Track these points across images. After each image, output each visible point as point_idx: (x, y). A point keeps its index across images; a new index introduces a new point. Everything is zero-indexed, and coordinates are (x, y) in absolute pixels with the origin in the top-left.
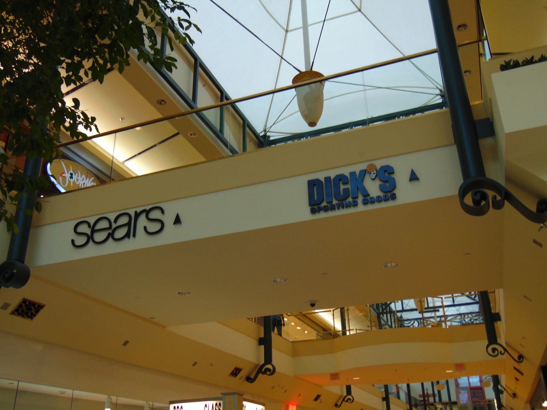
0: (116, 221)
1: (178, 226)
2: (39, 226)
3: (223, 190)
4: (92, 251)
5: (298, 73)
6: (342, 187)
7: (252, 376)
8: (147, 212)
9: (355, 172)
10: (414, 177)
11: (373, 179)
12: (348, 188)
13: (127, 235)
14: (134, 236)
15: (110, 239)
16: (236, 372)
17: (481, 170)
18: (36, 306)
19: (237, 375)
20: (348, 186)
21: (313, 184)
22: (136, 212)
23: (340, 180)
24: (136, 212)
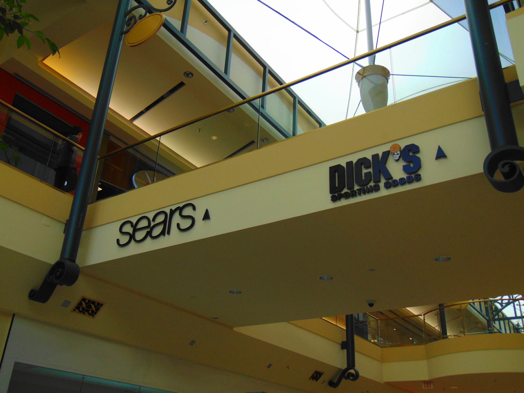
0: (154, 219)
1: (207, 221)
2: (90, 228)
4: (133, 249)
5: (361, 68)
6: (364, 171)
7: (335, 381)
8: (180, 209)
10: (441, 155)
11: (397, 160)
12: (370, 172)
13: (163, 233)
14: (169, 233)
15: (149, 238)
16: (316, 376)
17: (512, 137)
18: (96, 304)
19: (318, 379)
20: (371, 170)
21: (335, 170)
22: (171, 210)
23: (362, 164)
24: (171, 210)
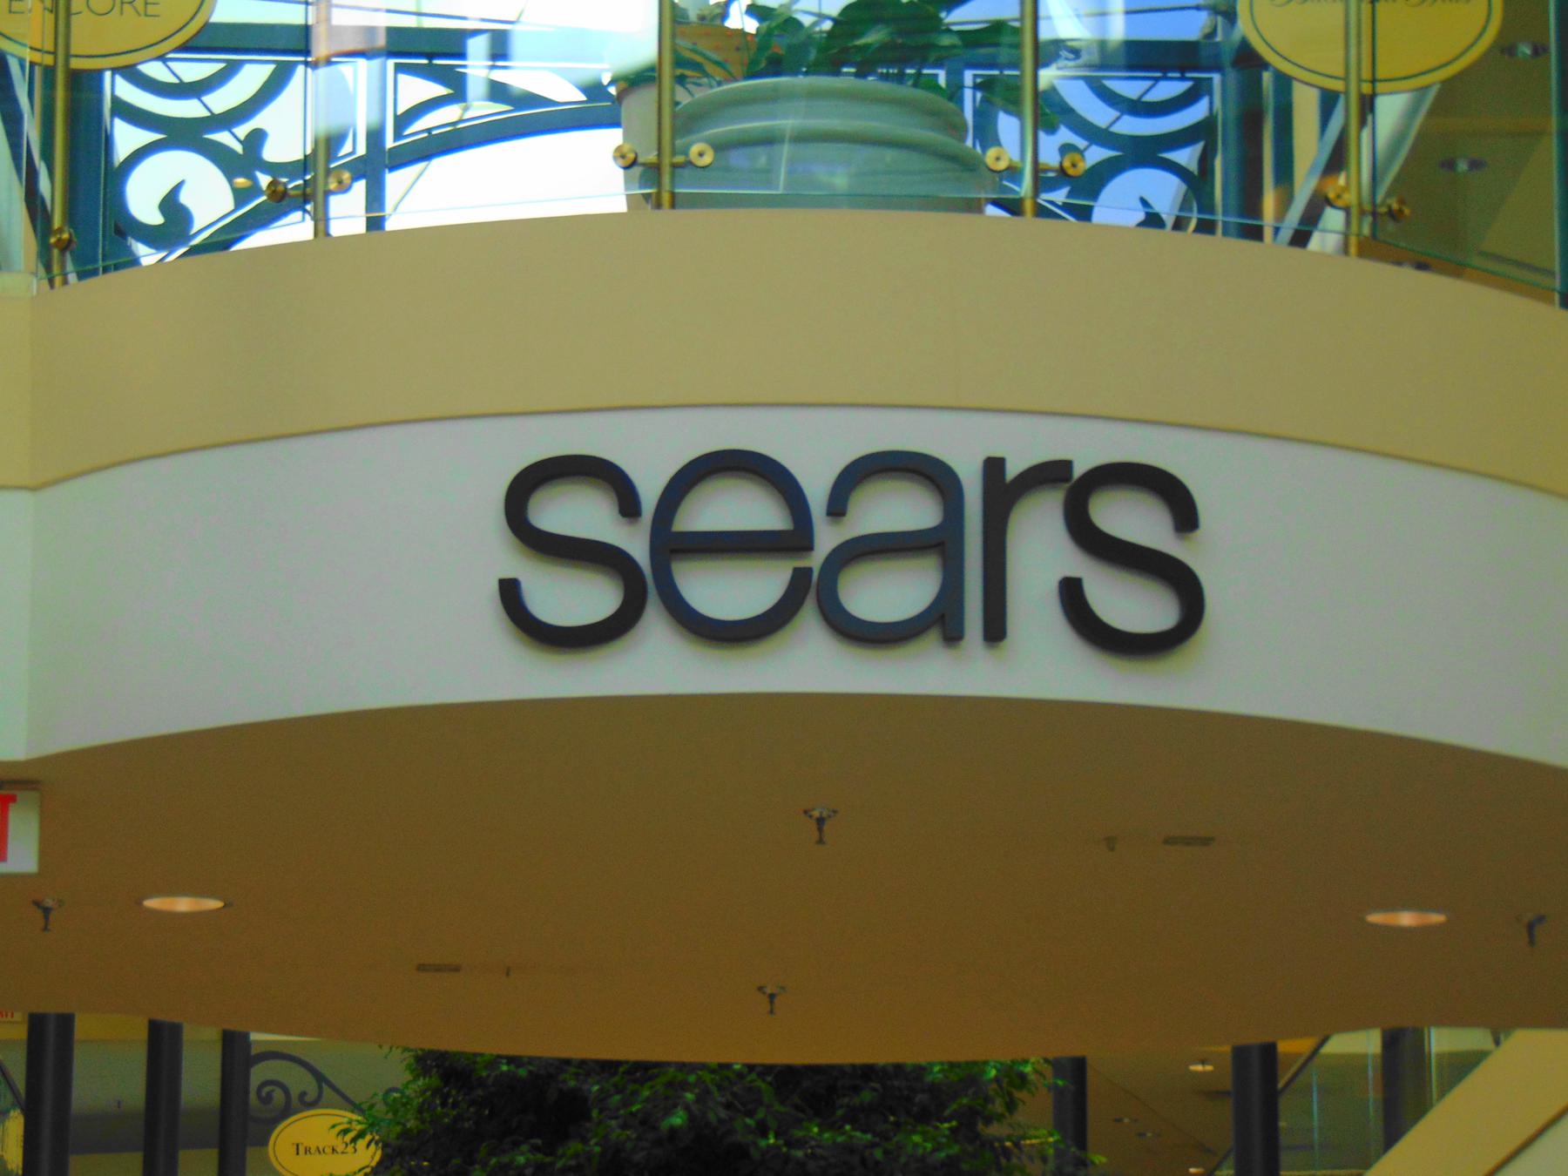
0: (837, 507)
3: (1531, 487)
8: (1076, 490)
9: (82, 275)
13: (941, 621)
14: (995, 630)
